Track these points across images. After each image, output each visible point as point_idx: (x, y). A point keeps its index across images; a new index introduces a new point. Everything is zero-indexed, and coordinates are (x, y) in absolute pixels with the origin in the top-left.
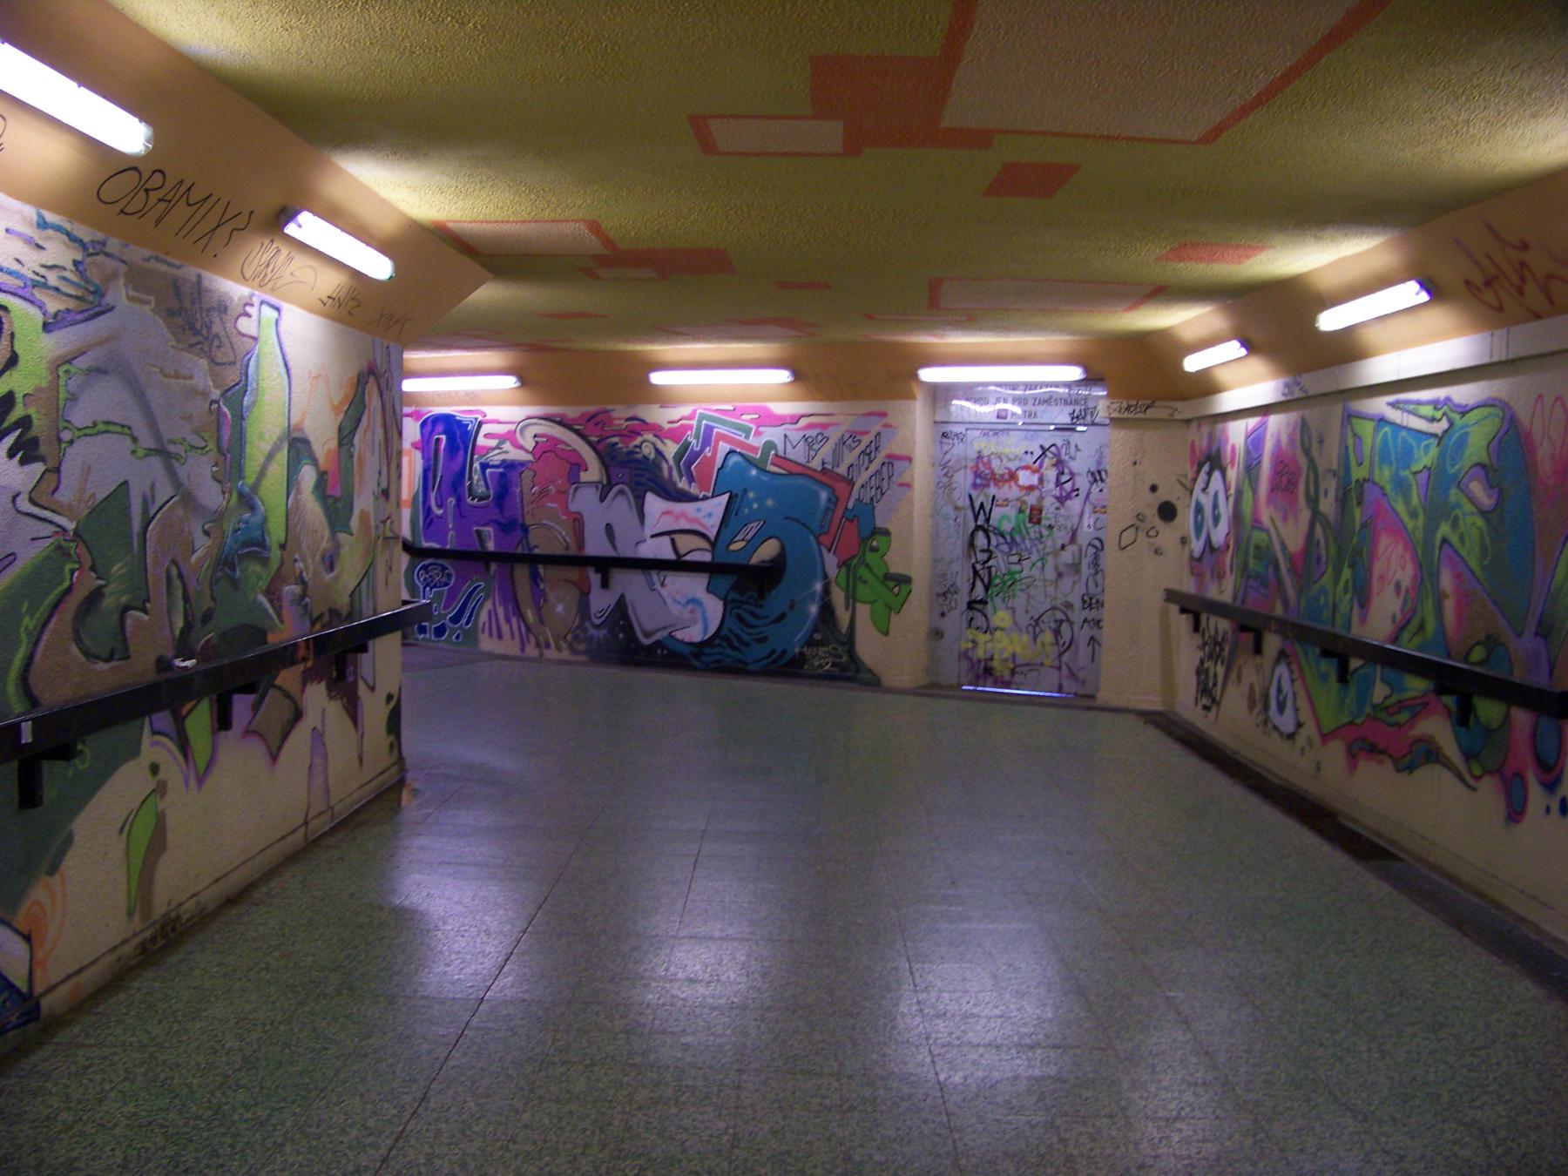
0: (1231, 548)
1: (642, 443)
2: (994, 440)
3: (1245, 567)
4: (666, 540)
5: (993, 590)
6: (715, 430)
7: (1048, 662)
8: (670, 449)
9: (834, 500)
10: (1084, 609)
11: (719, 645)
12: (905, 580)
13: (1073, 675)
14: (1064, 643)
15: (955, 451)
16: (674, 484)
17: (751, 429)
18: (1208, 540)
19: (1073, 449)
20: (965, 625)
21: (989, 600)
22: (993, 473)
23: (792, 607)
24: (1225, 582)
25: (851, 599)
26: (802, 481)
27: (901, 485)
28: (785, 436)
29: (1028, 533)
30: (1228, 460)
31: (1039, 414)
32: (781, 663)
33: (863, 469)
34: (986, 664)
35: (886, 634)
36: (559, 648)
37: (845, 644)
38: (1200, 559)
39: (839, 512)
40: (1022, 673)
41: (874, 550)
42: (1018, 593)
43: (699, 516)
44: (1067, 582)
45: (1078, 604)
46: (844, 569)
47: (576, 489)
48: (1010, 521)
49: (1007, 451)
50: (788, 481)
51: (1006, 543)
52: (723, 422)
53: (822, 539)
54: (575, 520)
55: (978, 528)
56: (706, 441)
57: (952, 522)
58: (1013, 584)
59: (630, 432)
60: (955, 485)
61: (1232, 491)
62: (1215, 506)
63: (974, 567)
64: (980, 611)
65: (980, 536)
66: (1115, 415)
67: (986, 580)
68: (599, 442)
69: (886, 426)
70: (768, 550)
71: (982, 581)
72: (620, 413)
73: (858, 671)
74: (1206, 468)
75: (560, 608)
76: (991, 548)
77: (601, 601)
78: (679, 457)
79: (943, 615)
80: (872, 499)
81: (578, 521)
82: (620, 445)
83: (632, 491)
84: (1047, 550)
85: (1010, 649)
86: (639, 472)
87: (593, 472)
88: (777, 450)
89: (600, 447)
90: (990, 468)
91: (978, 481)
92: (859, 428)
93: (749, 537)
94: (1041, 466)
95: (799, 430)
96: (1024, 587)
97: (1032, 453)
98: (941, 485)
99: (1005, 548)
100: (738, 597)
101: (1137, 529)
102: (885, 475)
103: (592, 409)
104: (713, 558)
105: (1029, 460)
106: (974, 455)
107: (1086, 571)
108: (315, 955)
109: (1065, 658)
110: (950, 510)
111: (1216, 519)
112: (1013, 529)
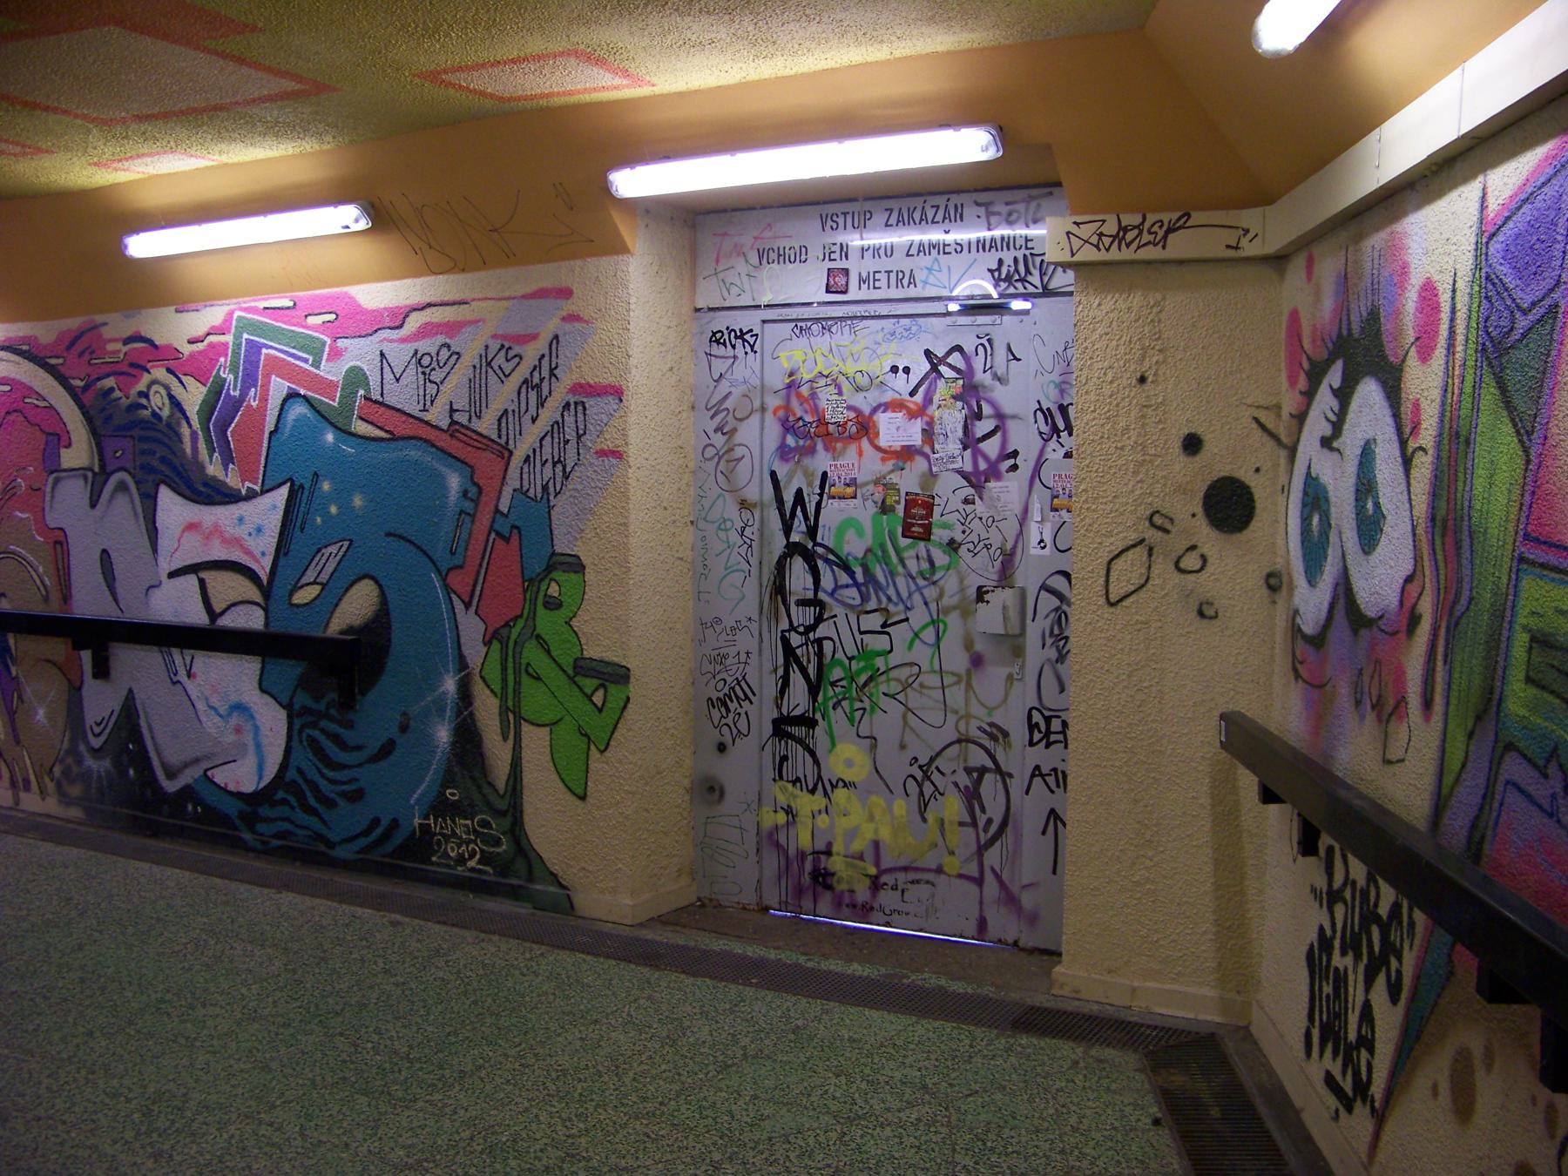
0: (1425, 627)
1: (149, 387)
2: (822, 342)
3: (1489, 705)
4: (191, 581)
5: (828, 694)
6: (264, 351)
7: (952, 864)
8: (193, 395)
9: (474, 492)
10: (1031, 744)
11: (284, 801)
12: (614, 676)
13: (1010, 899)
14: (990, 821)
15: (740, 372)
16: (202, 467)
17: (324, 344)
18: (1344, 589)
19: (1001, 354)
20: (769, 773)
21: (818, 716)
22: (822, 422)
23: (404, 728)
24: (1400, 732)
25: (513, 717)
26: (413, 453)
27: (602, 453)
28: (382, 354)
29: (902, 561)
30: (1410, 335)
31: (919, 276)
32: (389, 847)
33: (527, 419)
34: (816, 862)
35: (583, 798)
36: (43, 793)
37: (503, 814)
38: (1317, 641)
39: (484, 519)
40: (895, 888)
41: (553, 604)
42: (884, 702)
43: (242, 532)
44: (995, 674)
45: (1019, 733)
46: (496, 646)
47: (57, 481)
48: (860, 533)
49: (850, 368)
50: (389, 454)
51: (856, 584)
52: (276, 334)
53: (455, 579)
54: (56, 542)
55: (792, 549)
56: (250, 379)
57: (735, 538)
58: (871, 679)
59: (132, 365)
60: (739, 452)
61: (1427, 436)
62: (1365, 487)
63: (786, 642)
64: (800, 741)
65: (798, 565)
66: (1088, 254)
67: (812, 671)
68: (86, 388)
69: (572, 318)
70: (358, 605)
71: (804, 671)
72: (116, 327)
73: (530, 878)
74: (1334, 377)
75: (41, 714)
76: (821, 595)
77: (100, 702)
78: (208, 408)
79: (722, 748)
80: (545, 488)
81: (59, 542)
82: (117, 394)
83: (137, 483)
84: (946, 601)
85: (868, 832)
86: (146, 446)
87: (78, 453)
88: (368, 390)
89: (88, 398)
90: (815, 410)
91: (791, 441)
92: (517, 329)
93: (324, 578)
94: (928, 400)
95: (403, 340)
96: (894, 687)
97: (907, 370)
98: (710, 452)
99: (852, 595)
100: (309, 702)
101: (1150, 551)
102: (570, 434)
103: (74, 323)
104: (267, 624)
105: (902, 385)
106: (778, 381)
107: (1036, 652)
108: (158, 1082)
109: (992, 857)
110: (732, 510)
111: (1370, 529)
112: (869, 550)
